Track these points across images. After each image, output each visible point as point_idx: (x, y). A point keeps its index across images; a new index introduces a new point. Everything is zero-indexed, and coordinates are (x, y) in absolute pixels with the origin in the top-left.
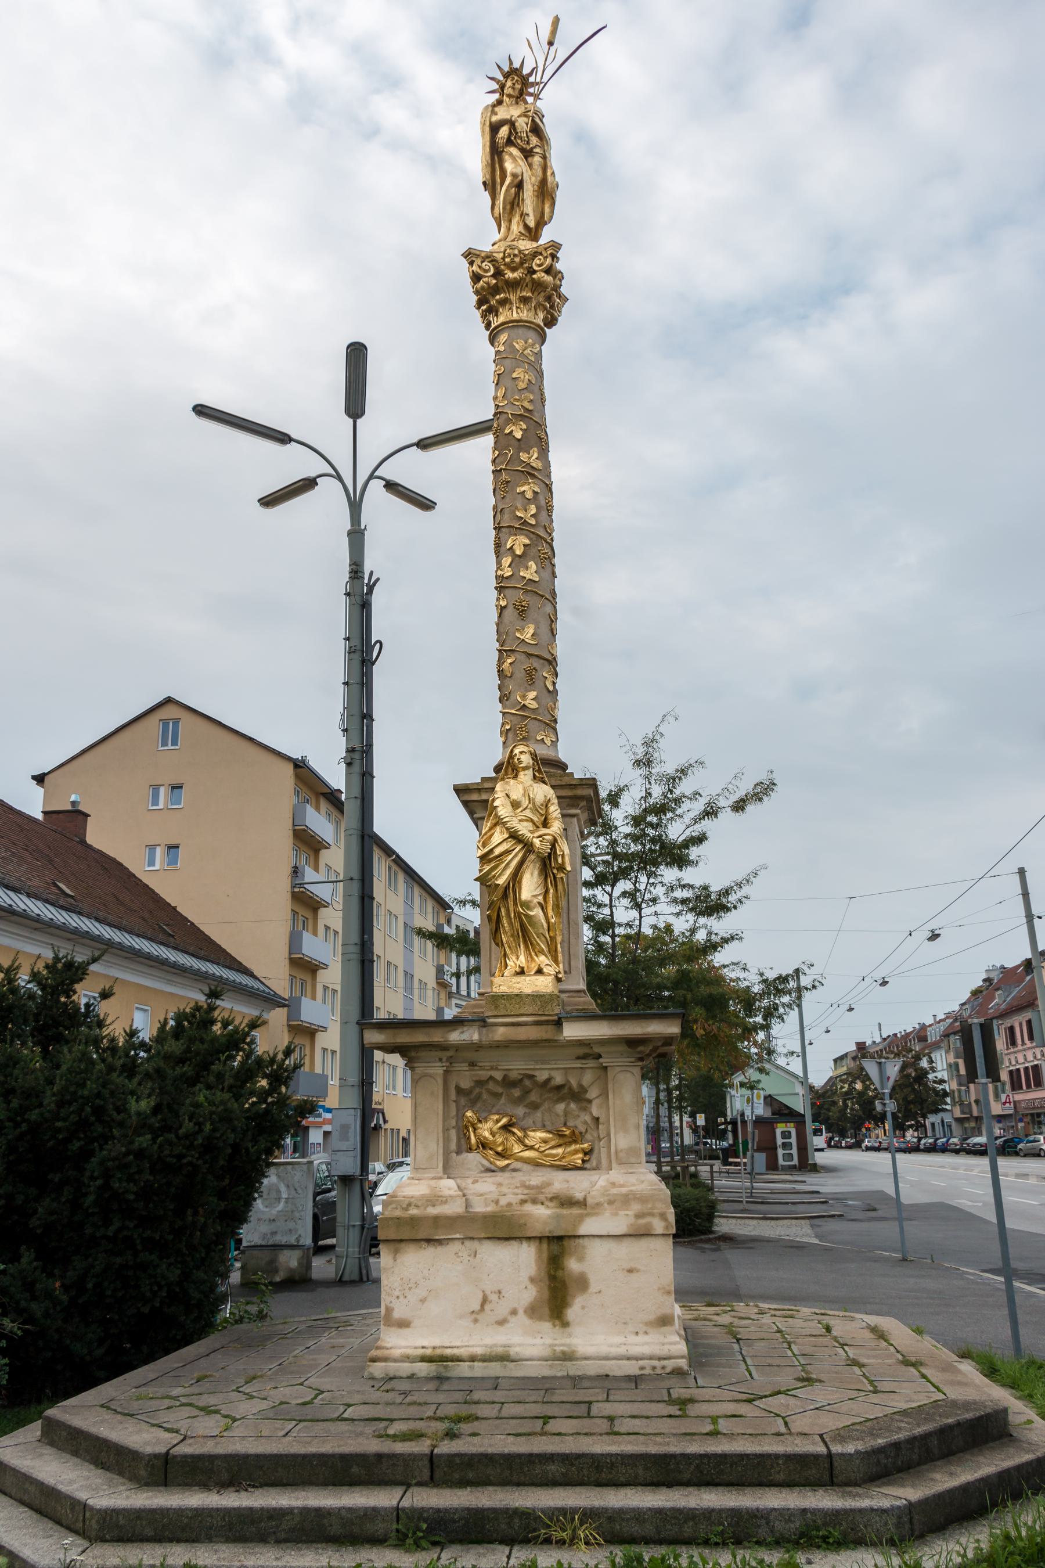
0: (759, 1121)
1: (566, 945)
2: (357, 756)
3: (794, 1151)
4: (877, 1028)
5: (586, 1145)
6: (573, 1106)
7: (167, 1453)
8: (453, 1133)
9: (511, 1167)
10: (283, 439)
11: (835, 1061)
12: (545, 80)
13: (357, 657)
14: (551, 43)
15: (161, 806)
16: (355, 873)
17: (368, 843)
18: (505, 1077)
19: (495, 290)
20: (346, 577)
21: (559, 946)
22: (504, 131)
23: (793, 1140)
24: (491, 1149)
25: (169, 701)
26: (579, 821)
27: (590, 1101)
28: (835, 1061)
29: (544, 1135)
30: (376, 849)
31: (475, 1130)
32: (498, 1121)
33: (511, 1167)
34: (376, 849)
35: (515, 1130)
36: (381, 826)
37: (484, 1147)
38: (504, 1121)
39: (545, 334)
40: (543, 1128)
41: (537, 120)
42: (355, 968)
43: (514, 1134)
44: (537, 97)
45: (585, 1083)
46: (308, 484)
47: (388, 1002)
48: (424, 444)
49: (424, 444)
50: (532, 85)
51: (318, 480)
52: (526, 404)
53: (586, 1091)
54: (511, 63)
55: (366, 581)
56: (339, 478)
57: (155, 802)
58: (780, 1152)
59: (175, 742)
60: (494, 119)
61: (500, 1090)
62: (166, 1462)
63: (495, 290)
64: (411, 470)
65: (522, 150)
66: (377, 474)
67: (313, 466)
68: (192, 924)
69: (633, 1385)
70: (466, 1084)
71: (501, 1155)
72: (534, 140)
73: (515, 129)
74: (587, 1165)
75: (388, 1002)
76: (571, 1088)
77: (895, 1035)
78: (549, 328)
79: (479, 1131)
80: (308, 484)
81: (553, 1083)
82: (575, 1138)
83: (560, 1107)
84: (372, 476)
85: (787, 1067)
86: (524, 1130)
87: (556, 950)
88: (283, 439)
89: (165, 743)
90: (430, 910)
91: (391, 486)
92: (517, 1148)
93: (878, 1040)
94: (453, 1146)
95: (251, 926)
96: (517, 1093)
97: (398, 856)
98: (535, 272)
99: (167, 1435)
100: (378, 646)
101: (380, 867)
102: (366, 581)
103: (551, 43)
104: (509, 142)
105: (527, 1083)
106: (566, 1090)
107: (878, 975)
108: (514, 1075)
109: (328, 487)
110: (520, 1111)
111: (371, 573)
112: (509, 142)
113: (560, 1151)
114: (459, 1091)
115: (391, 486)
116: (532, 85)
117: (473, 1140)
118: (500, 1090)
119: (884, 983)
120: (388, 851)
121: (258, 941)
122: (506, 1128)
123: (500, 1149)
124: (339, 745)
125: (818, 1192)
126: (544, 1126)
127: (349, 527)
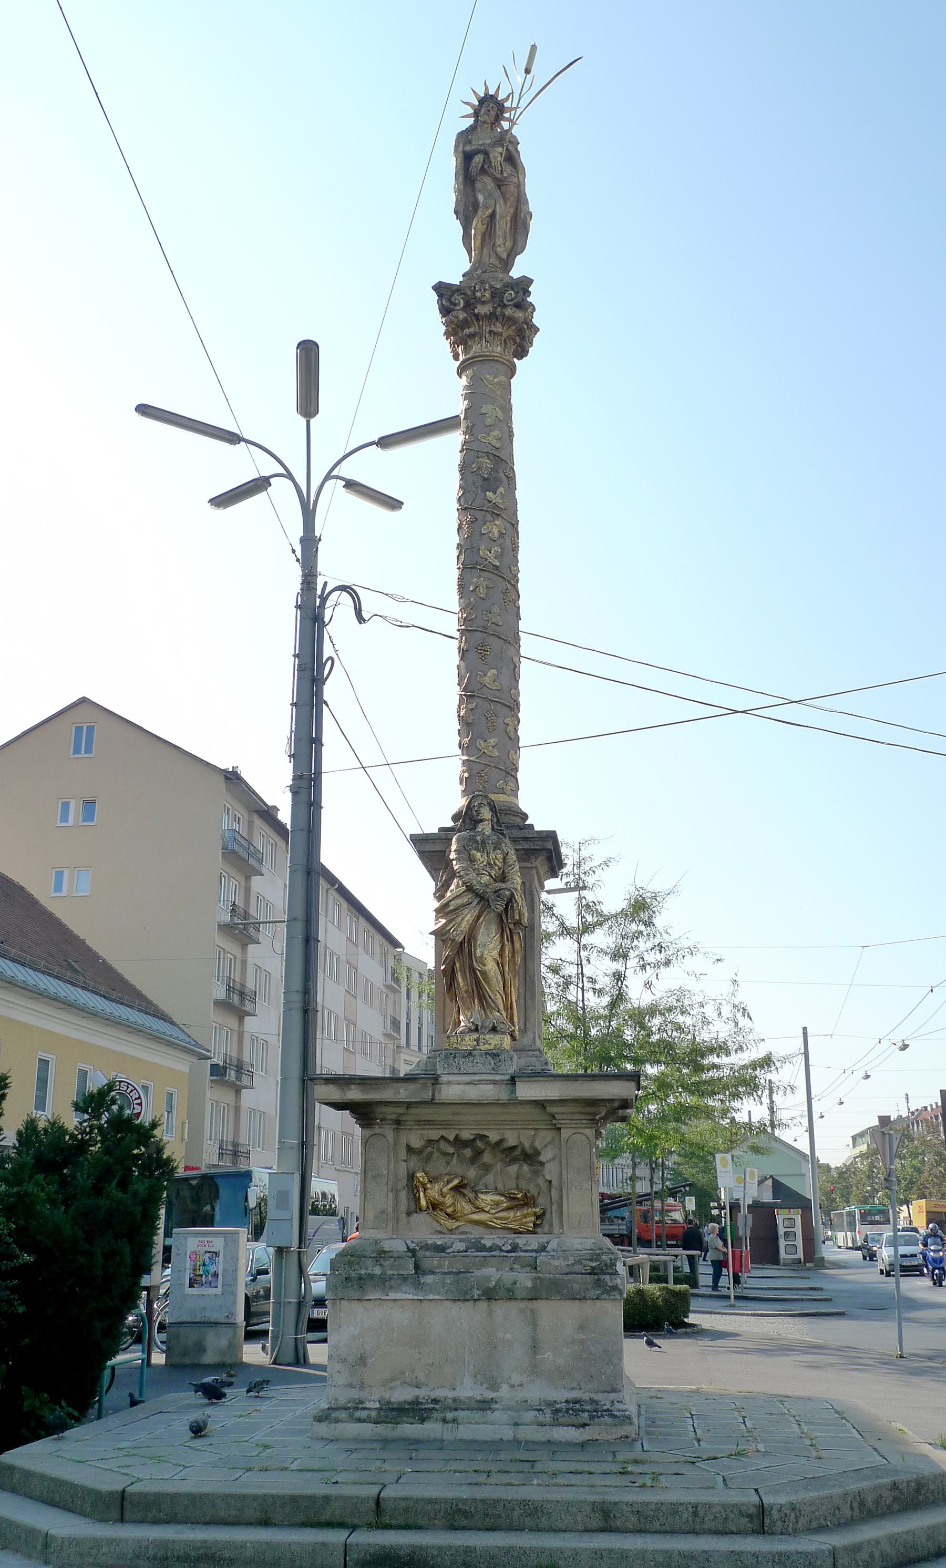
0: (756, 1207)
1: (522, 1001)
2: (304, 784)
3: (799, 1242)
4: (904, 1100)
5: (538, 1210)
6: (526, 1168)
7: (124, 1491)
8: (403, 1195)
9: (461, 1229)
10: (233, 438)
11: (854, 1138)
12: (523, 104)
13: (307, 674)
14: (527, 71)
15: (70, 823)
16: (300, 913)
17: (312, 876)
18: (457, 1137)
19: (465, 324)
20: (297, 588)
21: (514, 1004)
22: (478, 159)
23: (798, 1229)
24: (441, 1210)
25: (83, 701)
26: (538, 872)
27: (542, 1164)
28: (854, 1138)
29: (497, 1198)
30: (322, 881)
31: (425, 1189)
32: (448, 1182)
33: (461, 1229)
34: (322, 881)
35: (466, 1192)
36: (329, 857)
37: (434, 1209)
38: (456, 1182)
39: (515, 367)
40: (497, 1191)
41: (510, 148)
42: (297, 1016)
43: (465, 1195)
44: (512, 122)
45: (538, 1144)
46: (260, 485)
47: (330, 1059)
48: (385, 442)
49: (385, 442)
50: (510, 109)
51: (272, 480)
52: (495, 443)
53: (538, 1153)
54: (487, 89)
55: (319, 592)
56: (289, 476)
57: (65, 818)
58: (782, 1243)
59: (89, 750)
60: (468, 148)
61: (451, 1150)
62: (123, 1499)
63: (465, 324)
64: (372, 468)
65: (496, 180)
66: (334, 473)
67: (269, 467)
68: (104, 961)
69: (580, 1449)
70: (417, 1143)
71: (451, 1216)
72: (508, 170)
73: (489, 158)
74: (539, 1230)
75: (330, 1059)
76: (523, 1151)
77: (926, 1108)
78: (520, 358)
79: (429, 1191)
80: (260, 485)
81: (505, 1145)
82: (527, 1201)
83: (513, 1169)
84: (328, 477)
85: (795, 1145)
86: (476, 1192)
87: (511, 1007)
88: (233, 438)
89: (77, 750)
90: (377, 950)
91: (350, 485)
92: (468, 1208)
93: (905, 1114)
94: (403, 1207)
95: (173, 963)
96: (468, 1153)
97: (341, 885)
98: (504, 306)
99: (121, 1478)
100: (330, 662)
101: (327, 901)
102: (319, 592)
103: (527, 71)
104: (483, 170)
105: (479, 1144)
106: (518, 1152)
107: (898, 1037)
108: (466, 1135)
109: (281, 488)
110: (472, 1173)
111: (326, 583)
112: (483, 170)
113: (511, 1214)
114: (410, 1149)
115: (350, 485)
116: (510, 109)
117: (423, 1202)
118: (451, 1150)
119: (905, 1047)
120: (332, 880)
121: (182, 980)
122: (456, 1189)
123: (449, 1210)
124: (285, 772)
125: (821, 1289)
126: (496, 1189)
127: (302, 534)
